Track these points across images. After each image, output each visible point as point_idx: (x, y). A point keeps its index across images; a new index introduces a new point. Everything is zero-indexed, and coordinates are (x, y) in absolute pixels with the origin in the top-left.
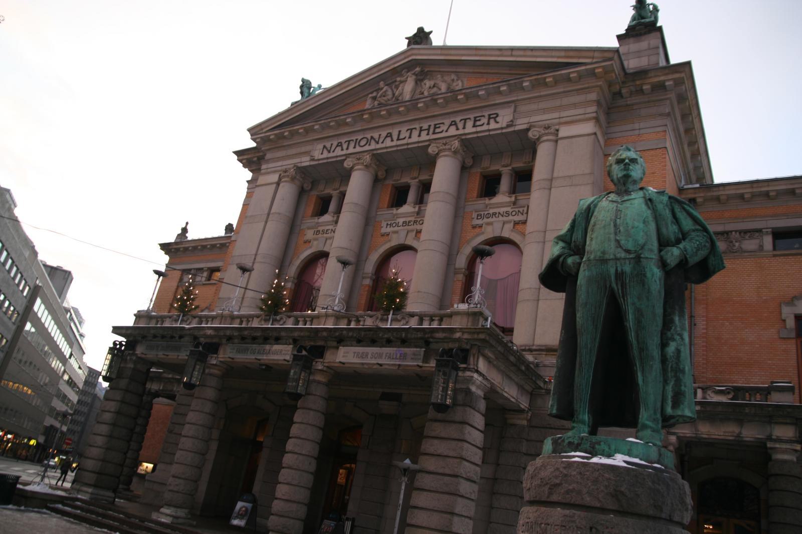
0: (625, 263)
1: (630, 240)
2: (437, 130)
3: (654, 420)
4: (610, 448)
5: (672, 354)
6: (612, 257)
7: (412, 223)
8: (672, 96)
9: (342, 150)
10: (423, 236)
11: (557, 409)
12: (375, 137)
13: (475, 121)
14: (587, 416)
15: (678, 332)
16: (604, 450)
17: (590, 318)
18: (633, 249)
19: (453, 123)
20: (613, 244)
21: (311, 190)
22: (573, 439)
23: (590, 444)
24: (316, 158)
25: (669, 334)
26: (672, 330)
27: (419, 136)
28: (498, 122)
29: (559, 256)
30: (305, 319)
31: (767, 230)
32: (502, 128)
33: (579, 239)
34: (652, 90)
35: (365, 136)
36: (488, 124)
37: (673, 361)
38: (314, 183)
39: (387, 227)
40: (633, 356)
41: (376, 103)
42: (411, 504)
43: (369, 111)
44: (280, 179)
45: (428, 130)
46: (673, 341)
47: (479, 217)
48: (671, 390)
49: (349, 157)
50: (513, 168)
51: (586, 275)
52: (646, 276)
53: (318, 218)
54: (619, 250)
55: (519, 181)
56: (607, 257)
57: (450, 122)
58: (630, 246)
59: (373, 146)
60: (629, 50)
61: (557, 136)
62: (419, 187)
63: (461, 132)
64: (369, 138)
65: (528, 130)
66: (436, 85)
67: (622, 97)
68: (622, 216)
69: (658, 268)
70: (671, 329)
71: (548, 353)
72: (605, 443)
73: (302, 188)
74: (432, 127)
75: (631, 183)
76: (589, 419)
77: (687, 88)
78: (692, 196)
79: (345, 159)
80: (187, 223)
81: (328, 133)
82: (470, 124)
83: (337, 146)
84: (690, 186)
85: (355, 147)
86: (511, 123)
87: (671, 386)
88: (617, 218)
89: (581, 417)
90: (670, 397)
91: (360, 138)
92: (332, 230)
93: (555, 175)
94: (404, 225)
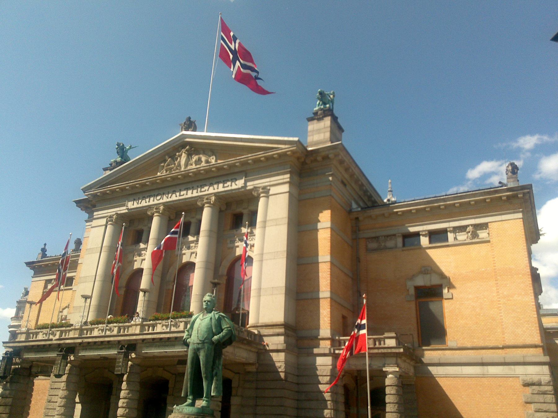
7: (193, 247)
9: (146, 202)
27: (192, 193)
31: (399, 235)
32: (239, 189)
35: (160, 193)
36: (231, 186)
44: (107, 222)
47: (231, 242)
53: (136, 246)
60: (313, 128)
63: (216, 191)
73: (169, 217)
80: (45, 245)
85: (154, 201)
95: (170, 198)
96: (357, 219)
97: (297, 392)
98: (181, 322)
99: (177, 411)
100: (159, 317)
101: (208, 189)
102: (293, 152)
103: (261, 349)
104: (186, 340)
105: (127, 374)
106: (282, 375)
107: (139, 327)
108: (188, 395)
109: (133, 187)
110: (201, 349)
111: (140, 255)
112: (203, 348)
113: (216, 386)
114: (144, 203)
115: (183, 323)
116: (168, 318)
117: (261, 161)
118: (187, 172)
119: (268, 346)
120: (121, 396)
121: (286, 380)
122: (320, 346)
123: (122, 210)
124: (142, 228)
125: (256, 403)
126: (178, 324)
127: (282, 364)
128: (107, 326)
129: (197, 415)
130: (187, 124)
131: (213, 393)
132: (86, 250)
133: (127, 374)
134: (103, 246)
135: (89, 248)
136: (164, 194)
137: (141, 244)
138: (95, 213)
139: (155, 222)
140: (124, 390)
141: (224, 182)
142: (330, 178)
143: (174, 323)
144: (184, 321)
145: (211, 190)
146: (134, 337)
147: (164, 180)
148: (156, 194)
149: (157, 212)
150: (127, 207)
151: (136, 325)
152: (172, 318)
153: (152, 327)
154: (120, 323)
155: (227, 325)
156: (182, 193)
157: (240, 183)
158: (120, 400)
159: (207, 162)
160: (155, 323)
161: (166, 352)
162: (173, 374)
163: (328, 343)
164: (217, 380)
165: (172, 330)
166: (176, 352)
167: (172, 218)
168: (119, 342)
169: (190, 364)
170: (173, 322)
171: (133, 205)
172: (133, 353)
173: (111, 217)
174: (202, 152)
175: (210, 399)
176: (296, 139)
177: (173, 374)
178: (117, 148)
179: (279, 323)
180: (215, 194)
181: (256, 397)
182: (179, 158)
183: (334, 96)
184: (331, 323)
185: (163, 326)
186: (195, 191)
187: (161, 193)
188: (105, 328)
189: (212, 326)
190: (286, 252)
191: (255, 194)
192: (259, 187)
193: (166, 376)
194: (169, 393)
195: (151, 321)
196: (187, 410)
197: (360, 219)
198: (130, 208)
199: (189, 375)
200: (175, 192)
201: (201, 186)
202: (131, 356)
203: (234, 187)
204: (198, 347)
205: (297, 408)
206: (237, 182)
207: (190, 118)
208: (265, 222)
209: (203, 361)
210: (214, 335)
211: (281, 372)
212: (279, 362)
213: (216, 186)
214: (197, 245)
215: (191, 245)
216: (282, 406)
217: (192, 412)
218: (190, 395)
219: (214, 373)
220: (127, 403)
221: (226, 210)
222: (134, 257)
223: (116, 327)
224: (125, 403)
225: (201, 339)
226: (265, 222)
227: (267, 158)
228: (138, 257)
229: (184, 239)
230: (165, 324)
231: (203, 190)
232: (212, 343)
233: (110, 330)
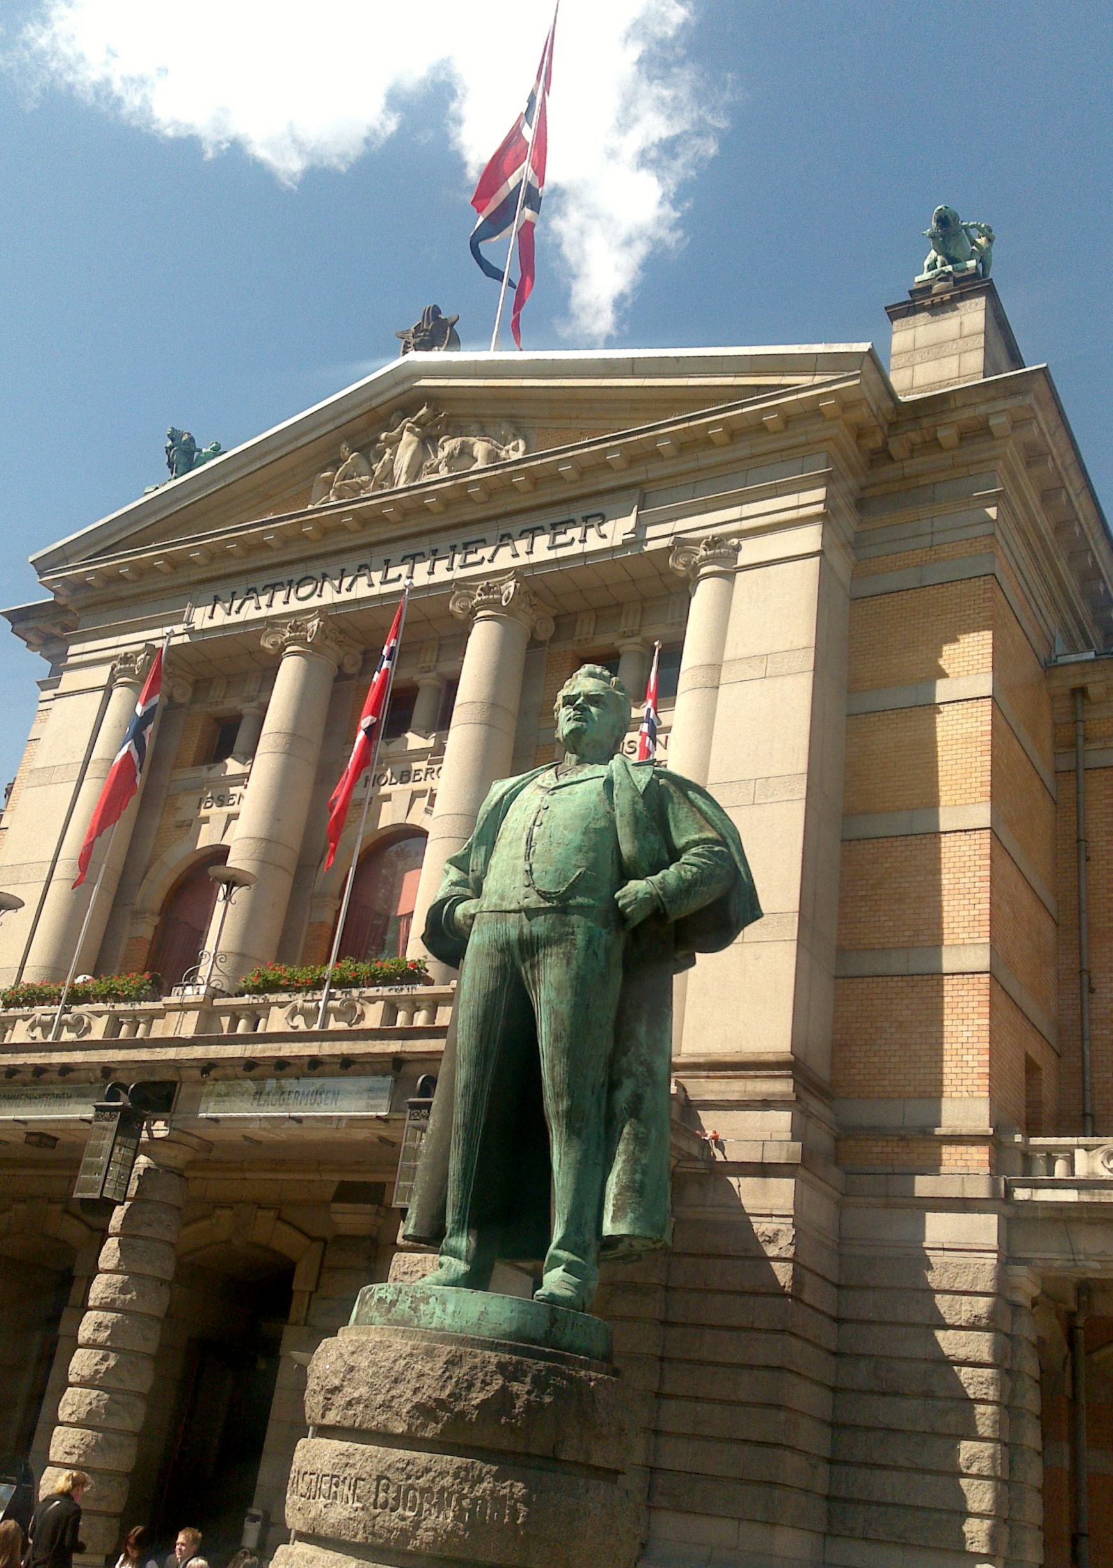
4: (444, 1311)
5: (624, 1105)
7: (422, 775)
8: (1010, 450)
14: (465, 1239)
15: (642, 1058)
23: (412, 1302)
25: (624, 1062)
26: (629, 1054)
28: (604, 537)
29: (442, 902)
32: (613, 549)
34: (961, 439)
38: (201, 685)
39: (365, 786)
44: (112, 678)
62: (440, 690)
63: (523, 560)
66: (467, 450)
67: (891, 458)
69: (605, 927)
70: (629, 1051)
71: (711, 1074)
77: (1045, 430)
78: (1078, 682)
80: (715, 1132)
84: (1073, 658)
90: (612, 1196)
93: (728, 654)
95: (349, 590)
96: (1080, 692)
97: (834, 1354)
98: (372, 1000)
100: (280, 978)
101: (493, 556)
102: (846, 403)
103: (692, 1158)
104: (453, 908)
105: (127, 1204)
106: (783, 1273)
107: (192, 1017)
108: (449, 1225)
109: (216, 555)
110: (548, 942)
111: (222, 801)
112: (558, 942)
113: (638, 1177)
114: (250, 611)
115: (380, 1004)
116: (318, 985)
117: (709, 442)
119: (720, 1145)
120: (92, 1295)
121: (796, 1296)
122: (943, 1169)
123: (174, 635)
124: (239, 708)
125: (662, 1381)
126: (358, 1006)
127: (782, 1227)
128: (66, 1011)
129: (513, 1350)
130: (426, 330)
131: (614, 1219)
132: (31, 771)
133: (127, 1204)
134: (93, 758)
135: (39, 765)
136: (325, 577)
137: (229, 761)
138: (73, 649)
139: (289, 672)
140: (107, 1271)
141: (556, 528)
142: (992, 512)
143: (342, 1003)
144: (382, 998)
145: (504, 559)
146: (170, 1053)
147: (327, 529)
148: (297, 578)
149: (293, 641)
150: (189, 624)
152: (333, 985)
153: (247, 1017)
154: (118, 999)
155: (701, 829)
156: (393, 573)
157: (618, 530)
158: (88, 1314)
159: (492, 456)
160: (261, 1001)
161: (299, 1120)
162: (313, 1239)
163: (979, 1155)
164: (640, 1141)
166: (344, 1124)
167: (349, 669)
168: (107, 1070)
169: (469, 1036)
170: (336, 1000)
171: (211, 617)
172: (159, 1120)
173: (126, 659)
174: (474, 427)
175: (593, 1256)
176: (864, 347)
177: (313, 1239)
178: (168, 450)
179: (771, 1058)
180: (518, 573)
181: (662, 1359)
182: (388, 451)
183: (990, 240)
184: (991, 1076)
185: (293, 1014)
186: (441, 565)
187: (317, 573)
188: (57, 1017)
189: (613, 822)
190: (805, 777)
191: (677, 564)
192: (696, 543)
193: (287, 1242)
194: (293, 1315)
195: (247, 996)
196: (450, 1308)
197: (1094, 691)
198: (197, 627)
199: (458, 1099)
200: (367, 571)
201: (466, 546)
202: (150, 1132)
203: (594, 543)
204: (526, 931)
205: (832, 1425)
206: (606, 528)
207: (436, 311)
208: (714, 668)
209: (554, 1013)
210: (625, 874)
211: (778, 1259)
212: (771, 1215)
213: (522, 545)
214: (436, 767)
215: (415, 766)
216: (779, 1407)
217: (479, 1326)
218: (457, 1231)
219: (623, 1096)
220: (115, 1327)
221: (553, 640)
222: (199, 808)
223: (100, 1016)
224: (107, 1327)
225: (546, 886)
226: (714, 668)
227: (735, 433)
228: (214, 805)
229: (388, 744)
230: (302, 1008)
231: (471, 558)
232: (617, 916)
233: (78, 1024)
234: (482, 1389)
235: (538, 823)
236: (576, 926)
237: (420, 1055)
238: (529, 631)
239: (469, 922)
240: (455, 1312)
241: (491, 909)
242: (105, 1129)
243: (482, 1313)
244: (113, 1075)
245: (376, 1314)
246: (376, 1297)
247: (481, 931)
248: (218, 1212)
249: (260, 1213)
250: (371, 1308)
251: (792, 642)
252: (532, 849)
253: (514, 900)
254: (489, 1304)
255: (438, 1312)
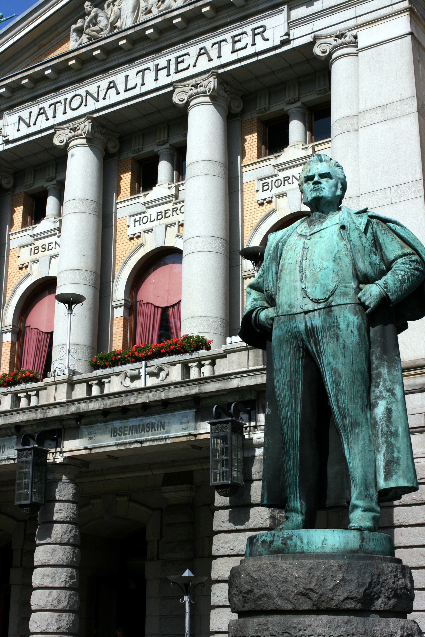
0: (314, 316)
1: (318, 285)
2: (181, 66)
3: (366, 497)
5: (381, 416)
6: (299, 310)
7: (170, 213)
10: (186, 231)
11: (268, 499)
12: (91, 92)
13: (234, 42)
14: (299, 502)
16: (296, 545)
17: (286, 388)
18: (321, 297)
19: (203, 51)
20: (299, 293)
21: (15, 186)
22: (266, 536)
23: (282, 540)
24: (11, 138)
26: (380, 386)
28: (267, 40)
30: (27, 393)
32: (275, 48)
33: (270, 287)
35: (78, 92)
37: (383, 424)
40: (337, 424)
41: (84, 39)
42: (211, 630)
43: (76, 53)
45: (168, 67)
46: (382, 400)
47: (266, 188)
48: (382, 458)
49: (59, 129)
50: (303, 103)
51: (277, 334)
52: (339, 328)
54: (307, 300)
55: (315, 120)
56: (294, 311)
57: (198, 50)
58: (318, 295)
59: (92, 105)
61: (357, 47)
63: (216, 63)
64: (84, 94)
65: (312, 44)
68: (309, 256)
69: (355, 315)
72: (296, 537)
73: (106, 150)
74: (173, 62)
75: (324, 205)
76: (301, 506)
79: (54, 133)
81: (22, 96)
82: (226, 48)
83: (39, 114)
86: (287, 37)
87: (382, 454)
88: (302, 259)
89: (292, 504)
90: (382, 467)
91: (69, 96)
92: (56, 243)
94: (159, 217)
99: (261, 549)
115: (179, 366)
118: (139, 28)
144: (179, 362)
151: (56, 383)
165: (149, 384)
167: (112, 150)
171: (18, 130)
172: (231, 474)
214: (179, 206)
217: (323, 547)
234: (332, 580)
235: (305, 258)
236: (338, 317)
237: (210, 394)
238: (227, 109)
239: (270, 322)
240: (308, 542)
241: (285, 314)
242: (26, 462)
243: (324, 540)
244: (22, 430)
245: (262, 549)
246: (260, 540)
247: (279, 327)
248: (93, 501)
249: (119, 499)
250: (258, 547)
251: (401, 95)
252: (304, 275)
253: (299, 307)
254: (327, 535)
255: (299, 544)
